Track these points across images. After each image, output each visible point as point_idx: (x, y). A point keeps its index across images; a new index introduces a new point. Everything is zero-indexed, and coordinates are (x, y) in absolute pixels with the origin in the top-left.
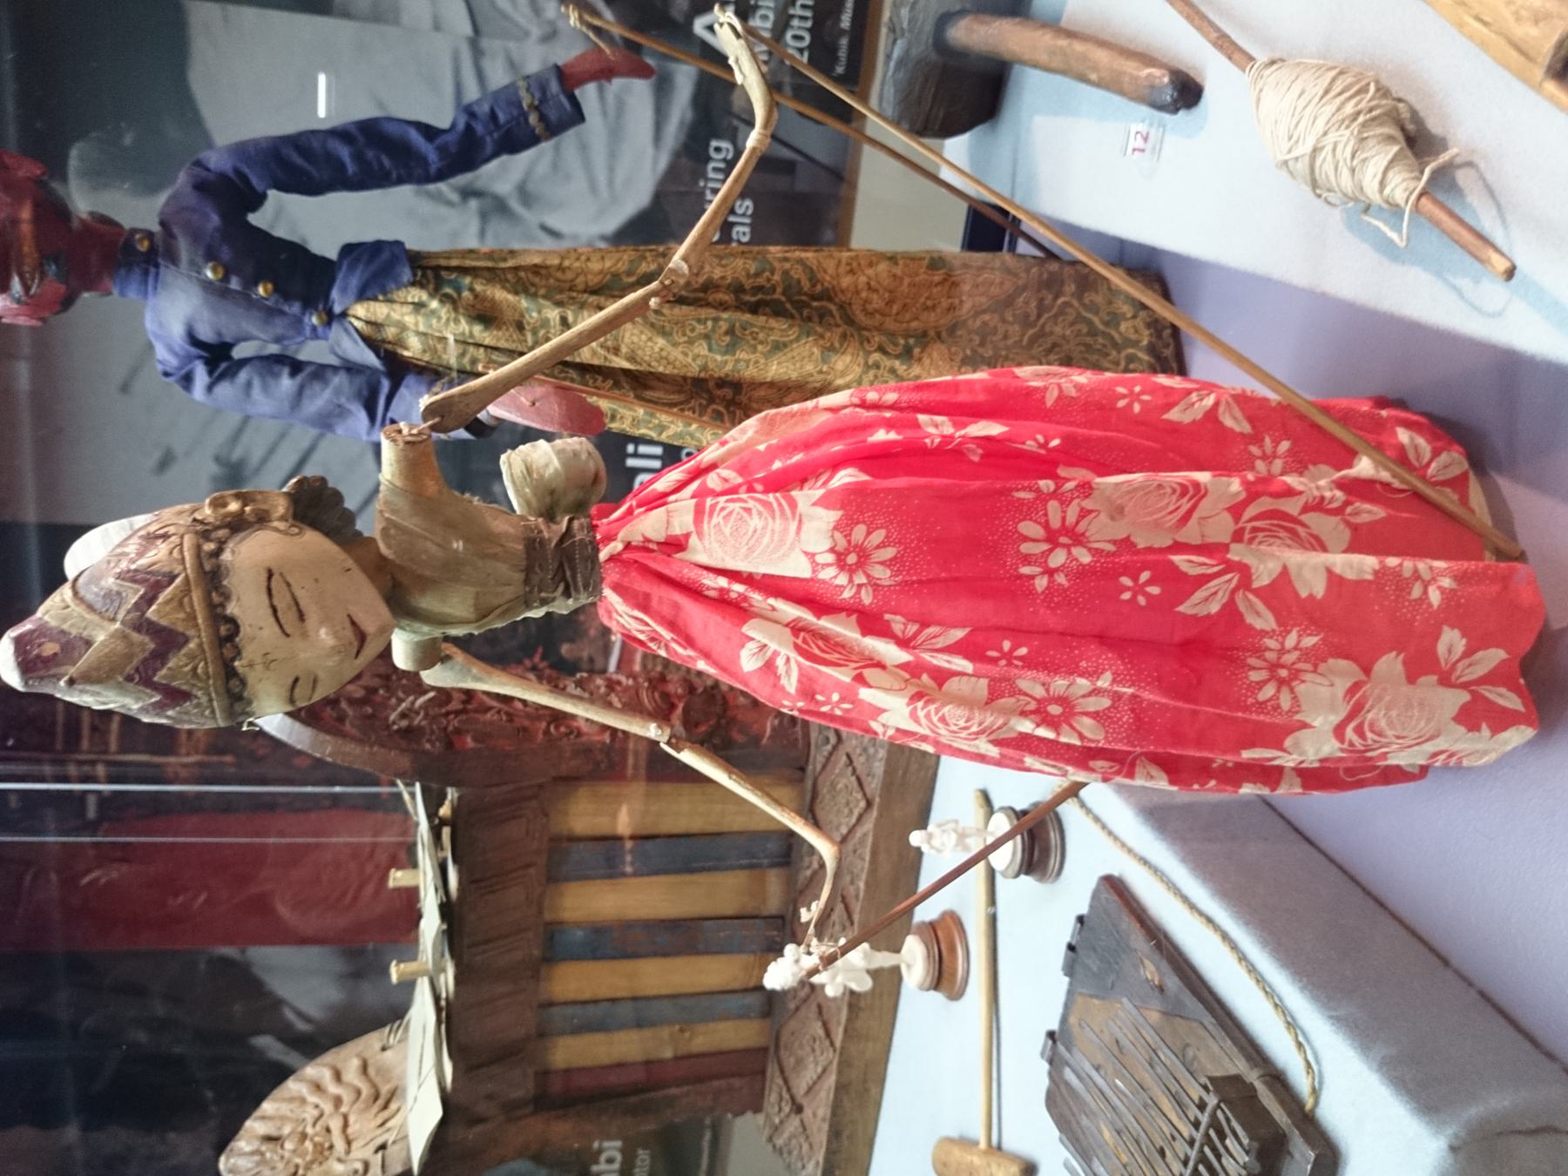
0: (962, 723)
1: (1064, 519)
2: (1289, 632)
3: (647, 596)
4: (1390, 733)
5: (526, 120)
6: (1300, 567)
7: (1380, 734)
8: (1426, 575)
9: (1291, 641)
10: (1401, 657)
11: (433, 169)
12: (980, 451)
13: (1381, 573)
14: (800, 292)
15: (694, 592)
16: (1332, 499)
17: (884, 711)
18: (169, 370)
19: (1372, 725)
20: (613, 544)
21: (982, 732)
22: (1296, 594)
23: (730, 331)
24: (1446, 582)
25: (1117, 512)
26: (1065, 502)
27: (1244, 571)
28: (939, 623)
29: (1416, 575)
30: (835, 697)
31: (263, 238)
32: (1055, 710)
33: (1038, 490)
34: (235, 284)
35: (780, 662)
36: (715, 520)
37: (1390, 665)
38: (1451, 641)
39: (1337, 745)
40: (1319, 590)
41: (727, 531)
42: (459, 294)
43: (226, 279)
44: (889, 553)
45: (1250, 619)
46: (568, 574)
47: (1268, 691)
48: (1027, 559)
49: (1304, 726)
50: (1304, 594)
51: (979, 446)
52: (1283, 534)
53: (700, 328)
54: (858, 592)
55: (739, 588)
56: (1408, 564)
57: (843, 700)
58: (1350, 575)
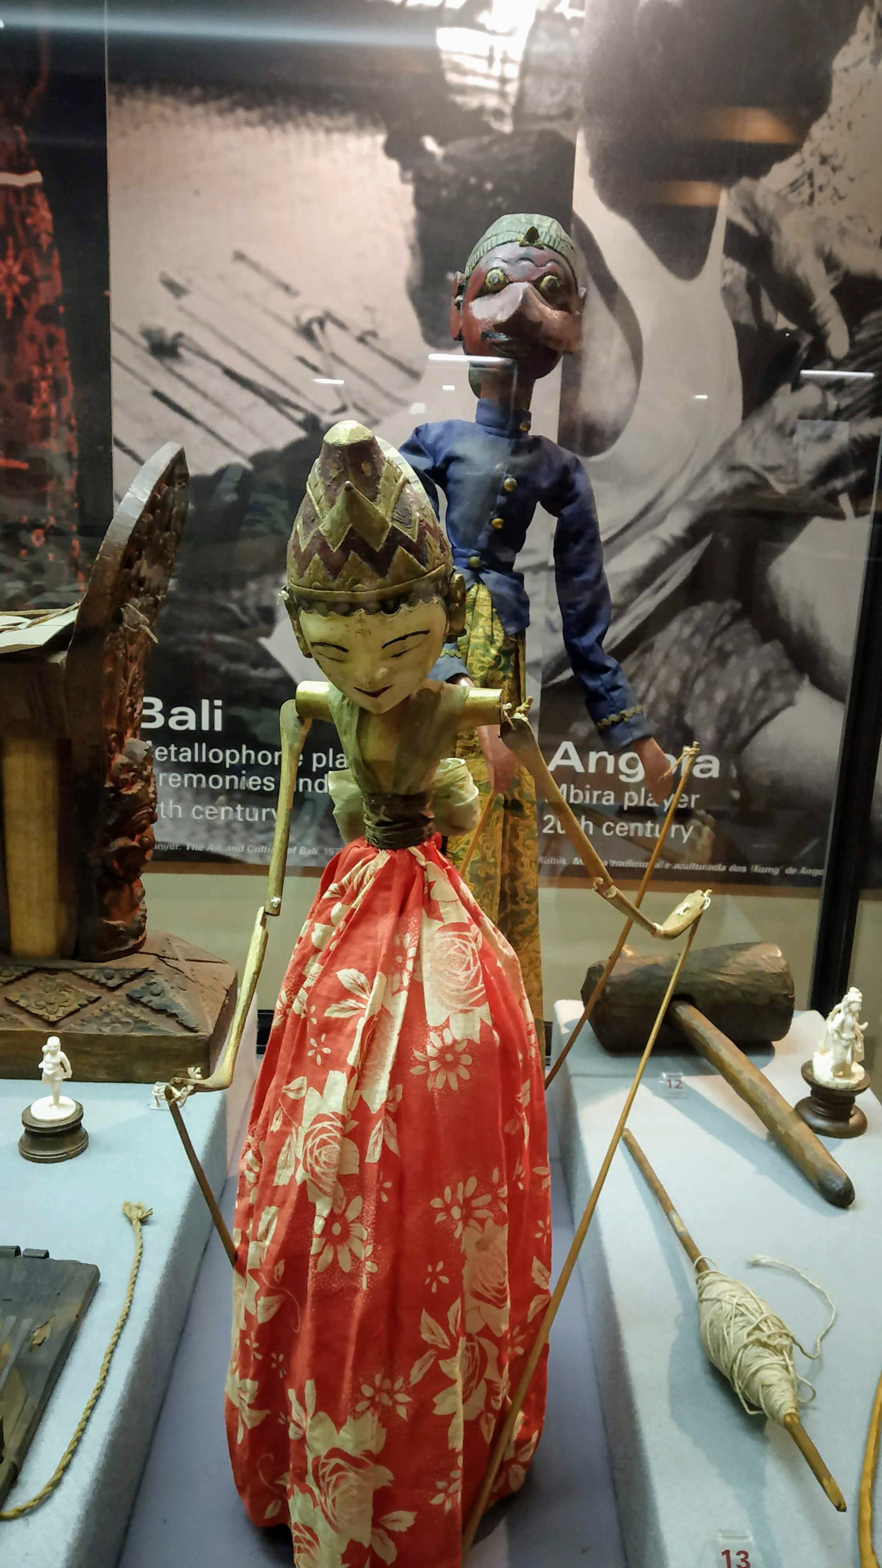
0: (323, 1159)
1: (478, 1208)
2: (409, 1395)
3: (389, 888)
4: (337, 1493)
5: (613, 712)
6: (455, 1393)
7: (336, 1486)
8: (451, 1490)
9: (402, 1398)
10: (390, 1485)
11: (575, 641)
12: (513, 1133)
13: (453, 1453)
14: (515, 924)
15: (399, 929)
16: (497, 1401)
17: (321, 1093)
18: (421, 435)
19: (343, 1477)
20: (423, 857)
21: (313, 1172)
22: (436, 1394)
23: (488, 877)
24: (448, 1506)
25: (482, 1246)
26: (490, 1206)
27: (450, 1353)
28: (398, 1129)
29: (451, 1482)
30: (326, 1050)
31: (526, 519)
32: (337, 1229)
33: (500, 1185)
34: (500, 499)
35: (351, 1003)
36: (457, 940)
37: (384, 1476)
38: (403, 1520)
39: (323, 1453)
40: (439, 1411)
41: (451, 952)
42: (501, 670)
43: (504, 493)
44: (454, 1085)
45: (417, 1364)
46: (400, 825)
47: (367, 1391)
48: (454, 1191)
49: (339, 1425)
50: (435, 1400)
51: (517, 1132)
52: (471, 1370)
53: (489, 853)
54: (421, 1063)
55: (410, 965)
56: (457, 1474)
57: (325, 1057)
58: (451, 1431)
